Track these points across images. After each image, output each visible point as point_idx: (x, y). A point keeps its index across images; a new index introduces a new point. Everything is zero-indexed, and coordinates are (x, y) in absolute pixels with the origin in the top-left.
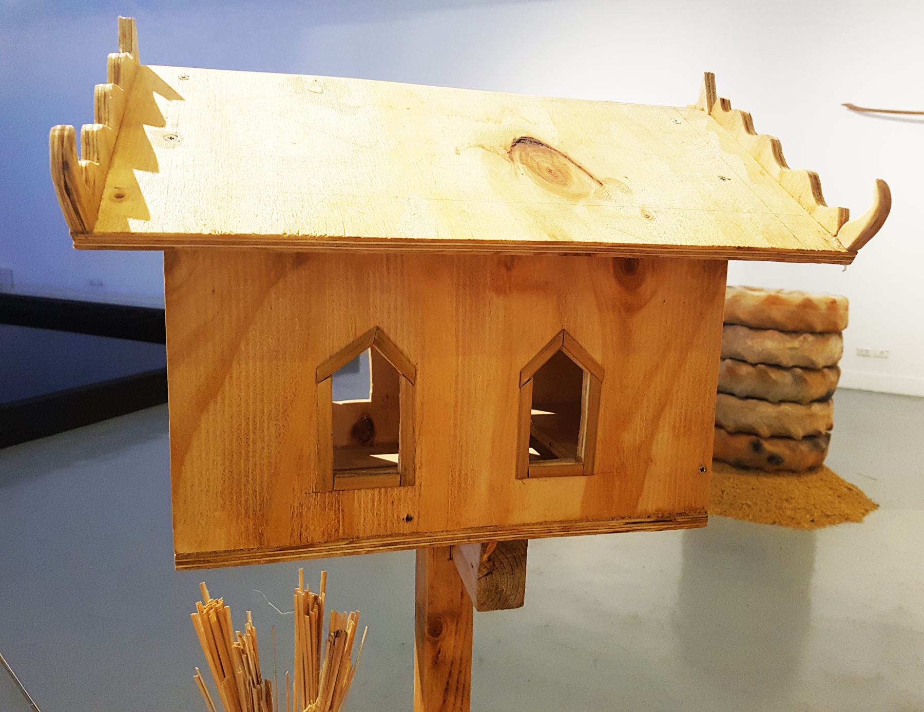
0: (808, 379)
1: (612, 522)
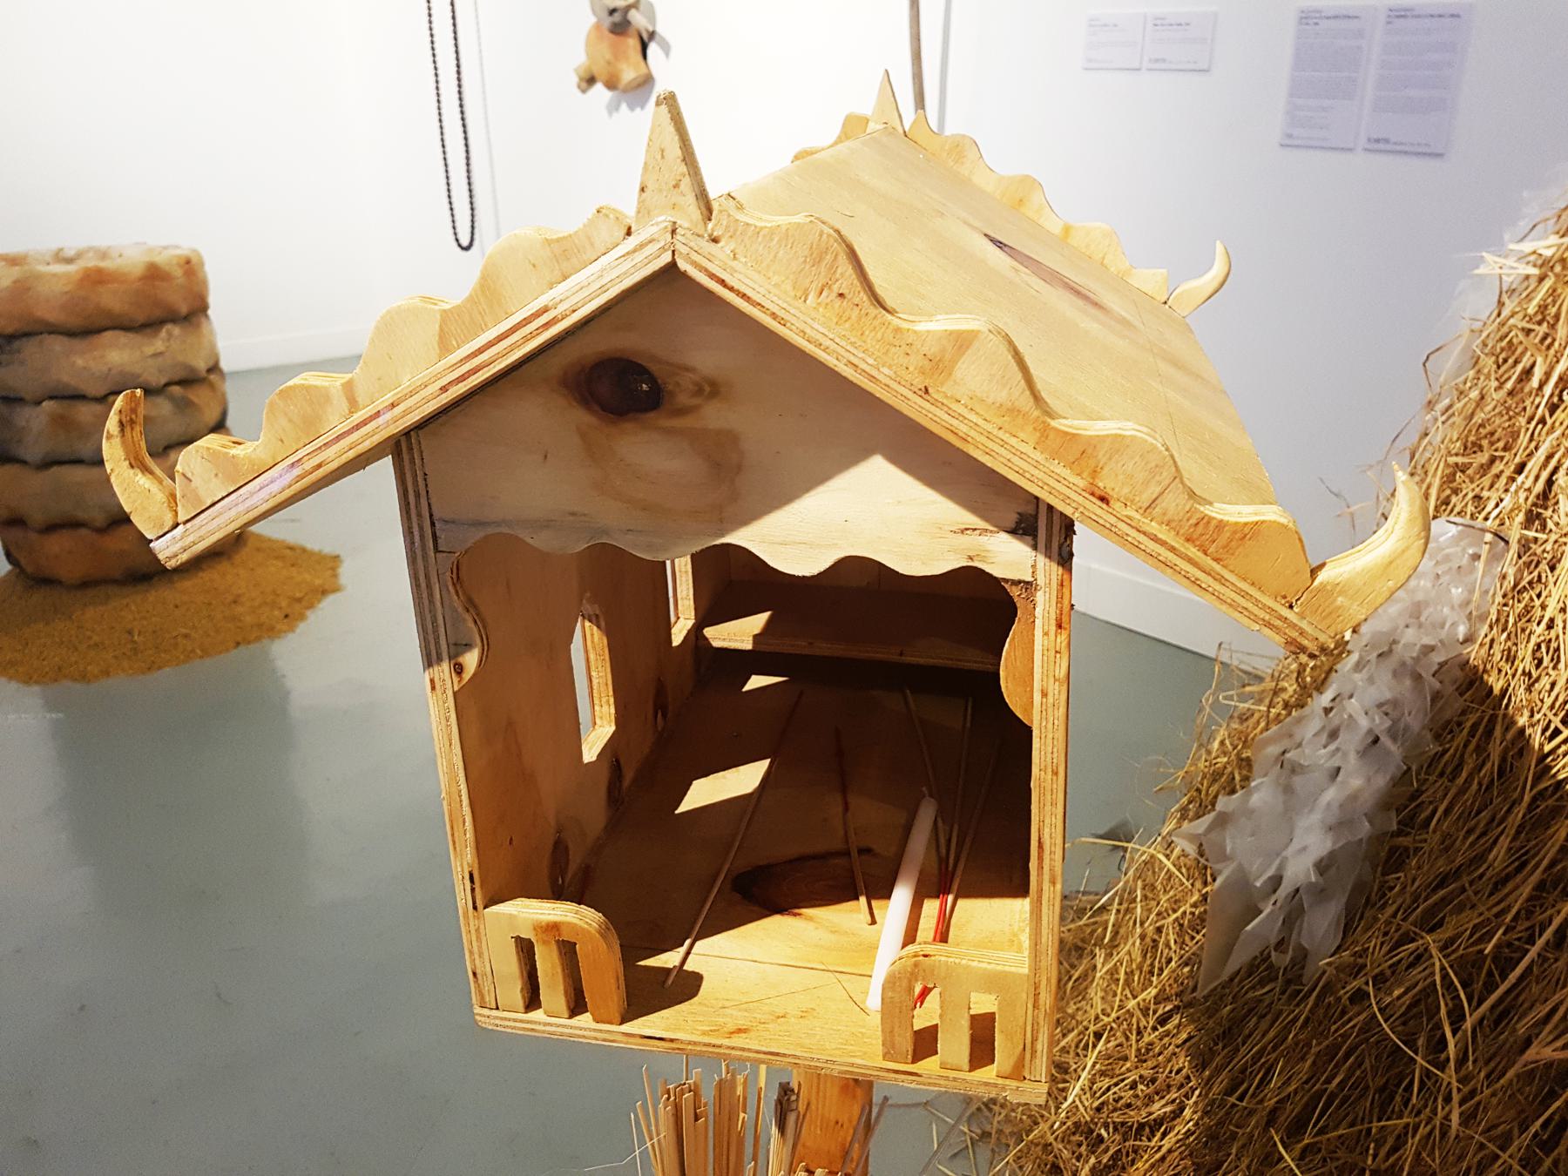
0: (195, 400)
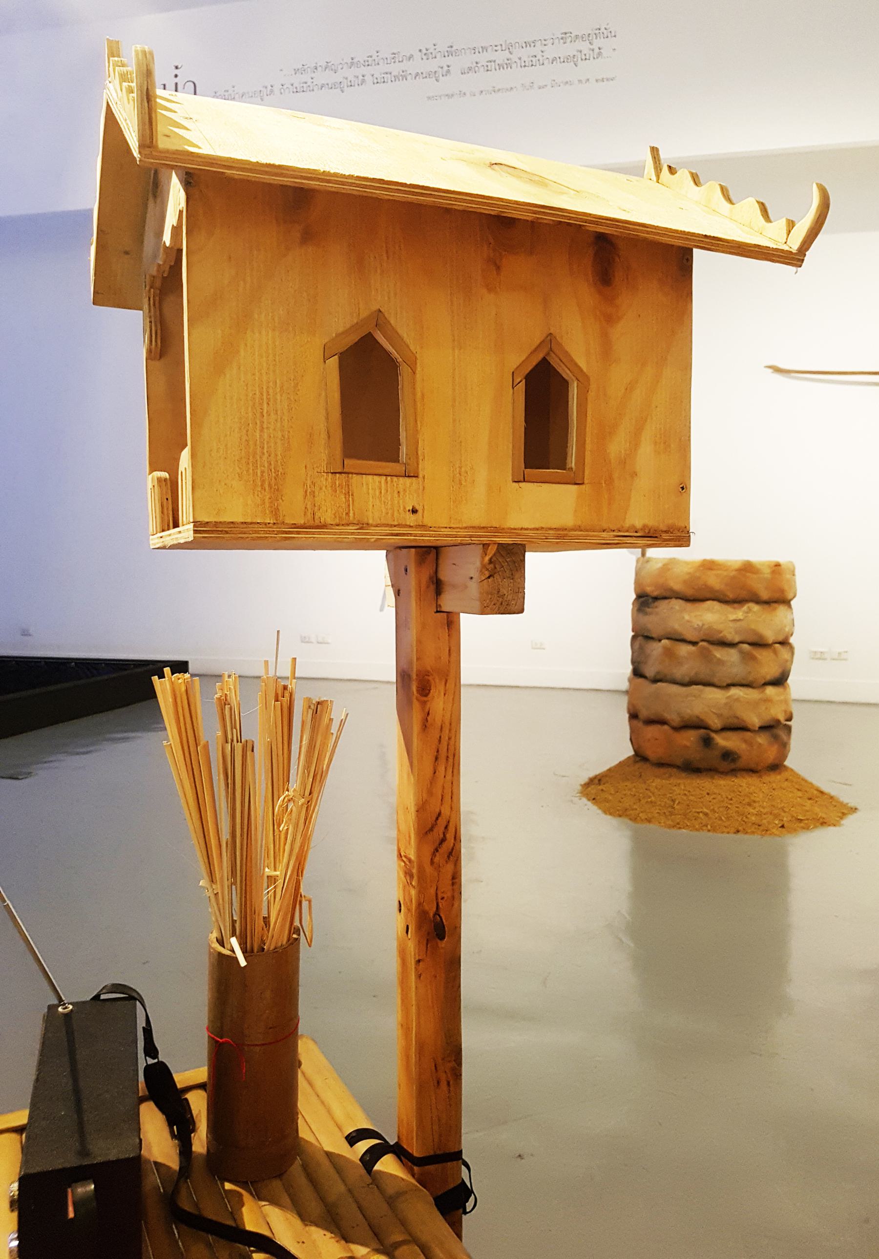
1: (603, 533)
